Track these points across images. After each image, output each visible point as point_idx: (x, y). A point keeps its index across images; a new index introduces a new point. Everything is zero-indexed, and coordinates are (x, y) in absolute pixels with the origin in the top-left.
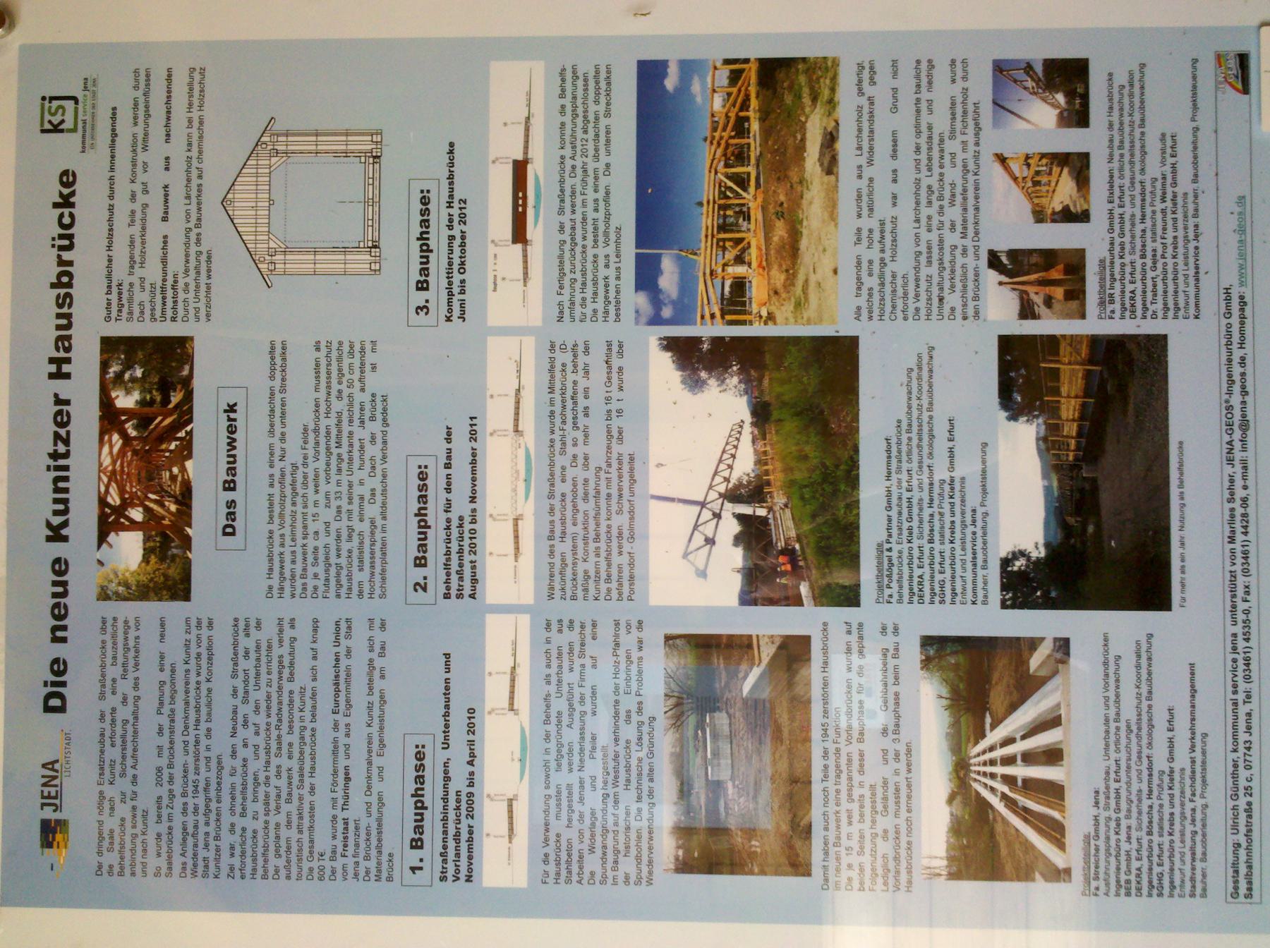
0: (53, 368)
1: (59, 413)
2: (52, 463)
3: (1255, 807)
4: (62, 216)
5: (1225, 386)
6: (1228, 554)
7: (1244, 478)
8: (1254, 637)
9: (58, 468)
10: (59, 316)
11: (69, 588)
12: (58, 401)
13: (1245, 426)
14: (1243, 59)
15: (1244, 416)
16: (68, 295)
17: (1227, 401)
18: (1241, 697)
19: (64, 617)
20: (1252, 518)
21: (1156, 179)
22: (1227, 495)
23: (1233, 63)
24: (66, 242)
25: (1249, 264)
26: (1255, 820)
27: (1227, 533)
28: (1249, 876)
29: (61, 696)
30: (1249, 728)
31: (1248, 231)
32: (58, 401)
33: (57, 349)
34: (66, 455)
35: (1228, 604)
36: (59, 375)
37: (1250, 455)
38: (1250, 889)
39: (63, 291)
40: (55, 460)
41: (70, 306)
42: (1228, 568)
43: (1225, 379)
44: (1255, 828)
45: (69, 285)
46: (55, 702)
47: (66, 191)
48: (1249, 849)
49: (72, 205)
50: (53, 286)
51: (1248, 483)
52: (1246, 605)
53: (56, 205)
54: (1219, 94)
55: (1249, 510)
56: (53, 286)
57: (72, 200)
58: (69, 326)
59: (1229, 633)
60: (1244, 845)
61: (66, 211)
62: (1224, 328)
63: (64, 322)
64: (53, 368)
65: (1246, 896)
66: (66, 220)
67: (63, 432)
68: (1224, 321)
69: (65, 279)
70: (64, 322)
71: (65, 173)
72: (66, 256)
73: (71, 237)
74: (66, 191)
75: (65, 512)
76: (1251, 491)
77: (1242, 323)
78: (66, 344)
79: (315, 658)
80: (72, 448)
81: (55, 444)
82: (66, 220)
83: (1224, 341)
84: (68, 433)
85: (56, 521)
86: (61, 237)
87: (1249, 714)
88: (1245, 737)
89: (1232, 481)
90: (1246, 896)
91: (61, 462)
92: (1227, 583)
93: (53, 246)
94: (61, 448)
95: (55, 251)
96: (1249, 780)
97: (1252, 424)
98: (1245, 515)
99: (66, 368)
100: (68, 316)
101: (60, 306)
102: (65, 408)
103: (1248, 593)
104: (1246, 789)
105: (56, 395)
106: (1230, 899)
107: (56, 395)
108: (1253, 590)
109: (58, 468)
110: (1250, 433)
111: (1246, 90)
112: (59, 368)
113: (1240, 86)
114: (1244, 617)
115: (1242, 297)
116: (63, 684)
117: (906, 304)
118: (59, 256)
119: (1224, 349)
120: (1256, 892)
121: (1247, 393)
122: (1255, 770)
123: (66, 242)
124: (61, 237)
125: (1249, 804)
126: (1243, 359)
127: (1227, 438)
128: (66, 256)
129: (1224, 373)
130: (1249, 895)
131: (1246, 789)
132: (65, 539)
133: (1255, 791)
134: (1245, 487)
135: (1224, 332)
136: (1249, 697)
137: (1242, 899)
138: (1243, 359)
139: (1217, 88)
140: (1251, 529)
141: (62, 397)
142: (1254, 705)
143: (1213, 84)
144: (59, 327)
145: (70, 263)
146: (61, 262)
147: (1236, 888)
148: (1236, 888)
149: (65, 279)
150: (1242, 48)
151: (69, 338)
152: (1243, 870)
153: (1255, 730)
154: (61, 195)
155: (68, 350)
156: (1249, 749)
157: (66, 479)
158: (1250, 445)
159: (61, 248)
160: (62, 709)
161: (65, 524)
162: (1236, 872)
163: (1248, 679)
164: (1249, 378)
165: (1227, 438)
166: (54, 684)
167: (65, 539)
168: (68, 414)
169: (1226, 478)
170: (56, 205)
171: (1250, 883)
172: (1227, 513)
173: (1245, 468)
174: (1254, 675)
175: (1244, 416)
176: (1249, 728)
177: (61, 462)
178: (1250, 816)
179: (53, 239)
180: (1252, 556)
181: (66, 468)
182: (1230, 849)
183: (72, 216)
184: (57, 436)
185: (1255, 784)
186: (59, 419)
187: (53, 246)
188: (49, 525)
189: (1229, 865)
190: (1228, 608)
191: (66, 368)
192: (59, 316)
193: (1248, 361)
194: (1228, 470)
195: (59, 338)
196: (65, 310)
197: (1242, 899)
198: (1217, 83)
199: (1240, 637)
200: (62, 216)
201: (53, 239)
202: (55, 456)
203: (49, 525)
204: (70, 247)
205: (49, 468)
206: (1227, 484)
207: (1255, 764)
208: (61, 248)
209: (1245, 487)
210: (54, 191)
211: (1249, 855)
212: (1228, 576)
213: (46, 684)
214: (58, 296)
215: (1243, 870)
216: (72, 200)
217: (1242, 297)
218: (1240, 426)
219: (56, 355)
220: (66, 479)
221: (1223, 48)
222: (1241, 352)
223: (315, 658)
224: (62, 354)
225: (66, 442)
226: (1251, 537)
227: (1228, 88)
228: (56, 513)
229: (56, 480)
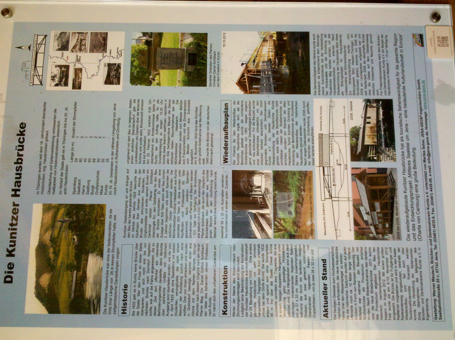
0: (13, 193)
1: (14, 209)
2: (10, 227)
3: (441, 286)
4: (20, 138)
5: (419, 111)
6: (423, 166)
7: (430, 172)
8: (436, 226)
9: (12, 229)
10: (17, 174)
11: (16, 243)
12: (14, 205)
13: (429, 155)
14: (421, 36)
15: (428, 152)
16: (21, 167)
17: (420, 116)
18: (431, 210)
19: (12, 268)
20: (433, 186)
21: (420, 313)
22: (422, 147)
23: (418, 37)
24: (21, 148)
25: (427, 102)
26: (441, 291)
27: (423, 159)
28: (440, 311)
29: (11, 277)
30: (437, 258)
31: (426, 92)
32: (14, 205)
33: (15, 186)
34: (16, 224)
35: (425, 183)
36: (15, 195)
37: (431, 164)
38: (441, 316)
39: (18, 165)
40: (12, 226)
41: (21, 170)
42: (424, 170)
43: (419, 109)
44: (441, 294)
45: (21, 163)
46: (8, 279)
47: (22, 130)
48: (439, 301)
49: (24, 135)
50: (15, 163)
51: (431, 174)
52: (433, 215)
53: (18, 135)
54: (414, 47)
55: (432, 183)
56: (15, 163)
57: (24, 133)
58: (20, 178)
59: (430, 248)
60: (438, 300)
61: (22, 137)
62: (418, 93)
63: (18, 176)
64: (13, 193)
65: (440, 319)
66: (22, 140)
67: (15, 216)
68: (418, 91)
69: (20, 161)
70: (18, 176)
71: (22, 124)
72: (21, 153)
73: (23, 146)
74: (22, 130)
75: (14, 245)
76: (432, 176)
77: (426, 121)
78: (19, 184)
79: (128, 173)
80: (18, 222)
81: (12, 220)
82: (22, 140)
83: (418, 97)
84: (17, 216)
85: (11, 249)
86: (19, 146)
87: (436, 253)
88: (433, 229)
89: (423, 142)
90: (440, 319)
91: (14, 227)
92: (424, 175)
93: (16, 149)
94: (14, 222)
95: (17, 151)
96: (438, 277)
97: (431, 154)
98: (431, 185)
99: (18, 193)
100: (20, 174)
101: (17, 170)
102: (17, 207)
103: (433, 211)
104: (437, 280)
105: (14, 203)
106: (434, 320)
107: (14, 203)
108: (435, 210)
109: (12, 229)
110: (431, 157)
111: (422, 45)
112: (15, 193)
113: (420, 44)
114: (433, 219)
115: (425, 113)
116: (12, 272)
117: (339, 294)
118: (18, 153)
119: (418, 99)
120: (443, 317)
121: (429, 144)
122: (440, 273)
123: (21, 148)
124: (19, 146)
125: (439, 285)
126: (427, 133)
127: (421, 128)
128: (21, 153)
129: (419, 107)
130: (440, 318)
131: (437, 280)
132: (13, 256)
133: (440, 281)
134: (430, 175)
135: (418, 94)
136: (436, 247)
137: (438, 320)
138: (427, 133)
139: (413, 45)
140: (433, 189)
141: (16, 203)
142: (438, 250)
143: (412, 43)
144: (16, 178)
145: (22, 155)
146: (19, 155)
147: (436, 316)
148: (436, 316)
149: (20, 161)
150: (421, 33)
151: (20, 182)
152: (438, 309)
153: (439, 259)
154: (20, 131)
155: (19, 186)
156: (437, 265)
157: (15, 233)
158: (431, 161)
159: (19, 150)
160: (11, 282)
161: (14, 250)
162: (436, 310)
163: (432, 204)
164: (429, 139)
165: (421, 128)
166: (9, 272)
167: (13, 256)
168: (18, 210)
169: (422, 141)
170: (18, 135)
171: (441, 314)
172: (422, 152)
173: (430, 169)
174: (434, 203)
175: (428, 152)
176: (437, 258)
177: (14, 227)
178: (439, 290)
179: (16, 147)
180: (437, 235)
181: (16, 229)
182: (433, 301)
183: (23, 139)
184: (13, 217)
185: (440, 278)
186: (14, 211)
187: (16, 149)
188: (8, 250)
189: (433, 307)
190: (425, 184)
191: (18, 193)
192: (17, 174)
193: (429, 133)
194: (422, 138)
195: (16, 182)
196: (19, 172)
197: (438, 320)
198: (413, 43)
199: (433, 241)
200: (20, 138)
201: (16, 147)
202: (12, 225)
203: (8, 250)
204: (22, 150)
205: (9, 229)
206: (422, 143)
207: (439, 271)
208: (19, 150)
209: (430, 175)
210: (18, 130)
211: (440, 303)
212: (424, 173)
213: (5, 272)
214: (17, 167)
215: (438, 309)
216: (24, 133)
217: (425, 113)
218: (428, 155)
219: (14, 188)
220: (15, 233)
221: (415, 32)
222: (426, 131)
223: (128, 173)
224: (17, 188)
225: (16, 220)
226: (433, 192)
227: (417, 45)
228: (11, 246)
229: (11, 234)
